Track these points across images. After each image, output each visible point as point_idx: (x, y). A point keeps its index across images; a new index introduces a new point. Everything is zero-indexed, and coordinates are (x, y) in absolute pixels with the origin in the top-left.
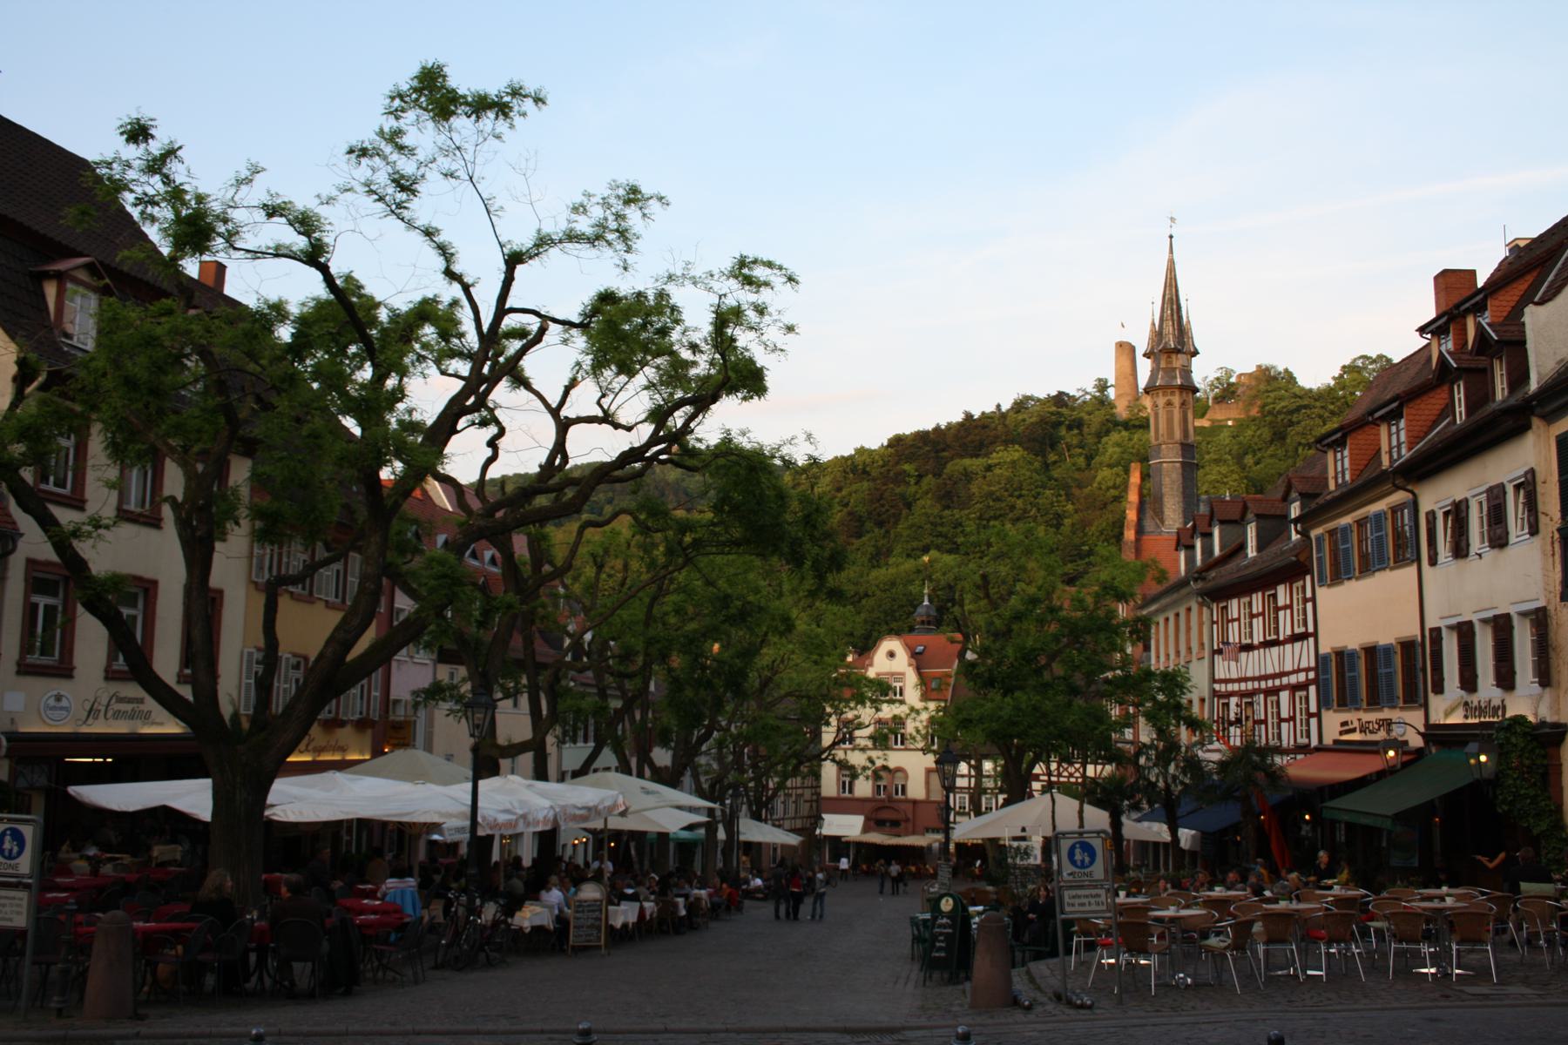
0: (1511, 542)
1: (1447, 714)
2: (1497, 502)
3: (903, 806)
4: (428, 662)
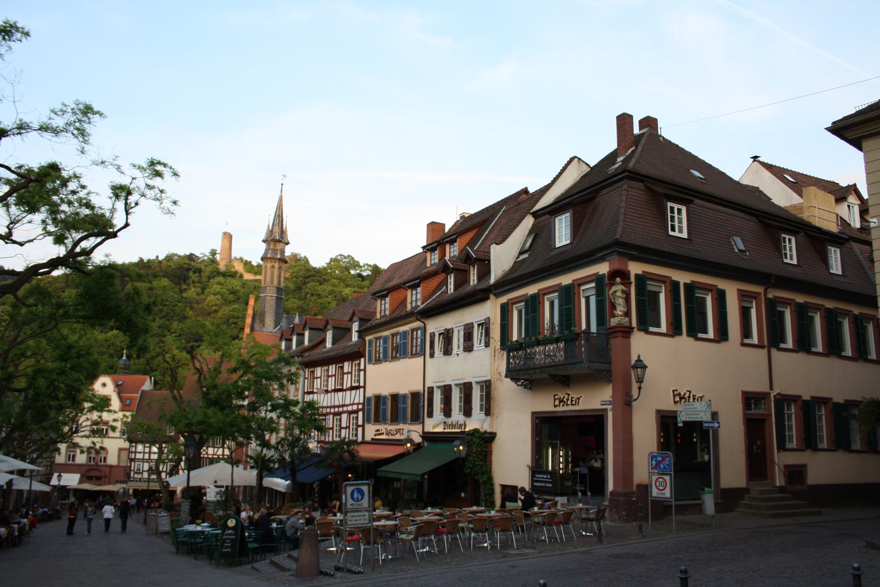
0: (474, 349)
1: (434, 427)
2: (470, 331)
3: (104, 469)
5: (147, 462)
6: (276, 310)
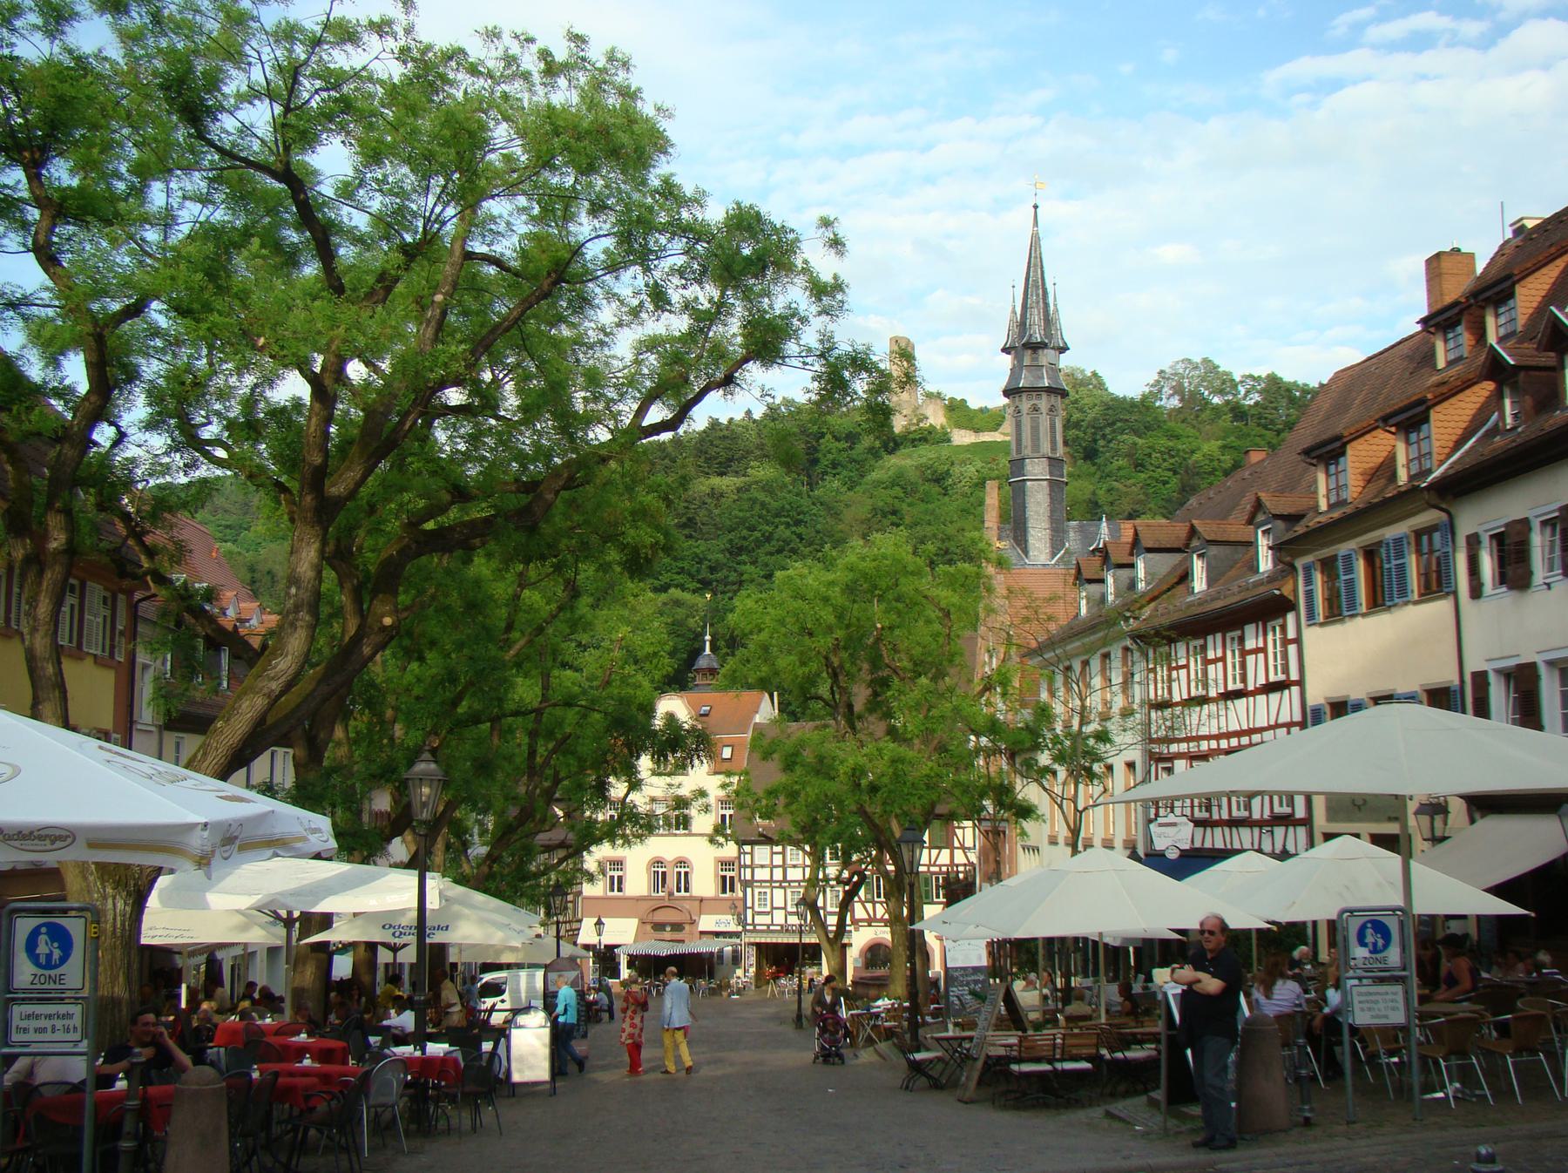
3: (687, 905)
4: (153, 729)
5: (780, 887)
6: (1052, 511)
